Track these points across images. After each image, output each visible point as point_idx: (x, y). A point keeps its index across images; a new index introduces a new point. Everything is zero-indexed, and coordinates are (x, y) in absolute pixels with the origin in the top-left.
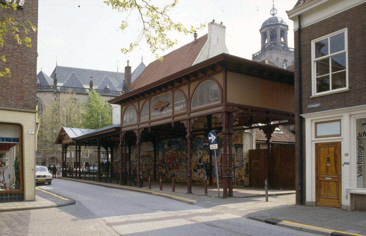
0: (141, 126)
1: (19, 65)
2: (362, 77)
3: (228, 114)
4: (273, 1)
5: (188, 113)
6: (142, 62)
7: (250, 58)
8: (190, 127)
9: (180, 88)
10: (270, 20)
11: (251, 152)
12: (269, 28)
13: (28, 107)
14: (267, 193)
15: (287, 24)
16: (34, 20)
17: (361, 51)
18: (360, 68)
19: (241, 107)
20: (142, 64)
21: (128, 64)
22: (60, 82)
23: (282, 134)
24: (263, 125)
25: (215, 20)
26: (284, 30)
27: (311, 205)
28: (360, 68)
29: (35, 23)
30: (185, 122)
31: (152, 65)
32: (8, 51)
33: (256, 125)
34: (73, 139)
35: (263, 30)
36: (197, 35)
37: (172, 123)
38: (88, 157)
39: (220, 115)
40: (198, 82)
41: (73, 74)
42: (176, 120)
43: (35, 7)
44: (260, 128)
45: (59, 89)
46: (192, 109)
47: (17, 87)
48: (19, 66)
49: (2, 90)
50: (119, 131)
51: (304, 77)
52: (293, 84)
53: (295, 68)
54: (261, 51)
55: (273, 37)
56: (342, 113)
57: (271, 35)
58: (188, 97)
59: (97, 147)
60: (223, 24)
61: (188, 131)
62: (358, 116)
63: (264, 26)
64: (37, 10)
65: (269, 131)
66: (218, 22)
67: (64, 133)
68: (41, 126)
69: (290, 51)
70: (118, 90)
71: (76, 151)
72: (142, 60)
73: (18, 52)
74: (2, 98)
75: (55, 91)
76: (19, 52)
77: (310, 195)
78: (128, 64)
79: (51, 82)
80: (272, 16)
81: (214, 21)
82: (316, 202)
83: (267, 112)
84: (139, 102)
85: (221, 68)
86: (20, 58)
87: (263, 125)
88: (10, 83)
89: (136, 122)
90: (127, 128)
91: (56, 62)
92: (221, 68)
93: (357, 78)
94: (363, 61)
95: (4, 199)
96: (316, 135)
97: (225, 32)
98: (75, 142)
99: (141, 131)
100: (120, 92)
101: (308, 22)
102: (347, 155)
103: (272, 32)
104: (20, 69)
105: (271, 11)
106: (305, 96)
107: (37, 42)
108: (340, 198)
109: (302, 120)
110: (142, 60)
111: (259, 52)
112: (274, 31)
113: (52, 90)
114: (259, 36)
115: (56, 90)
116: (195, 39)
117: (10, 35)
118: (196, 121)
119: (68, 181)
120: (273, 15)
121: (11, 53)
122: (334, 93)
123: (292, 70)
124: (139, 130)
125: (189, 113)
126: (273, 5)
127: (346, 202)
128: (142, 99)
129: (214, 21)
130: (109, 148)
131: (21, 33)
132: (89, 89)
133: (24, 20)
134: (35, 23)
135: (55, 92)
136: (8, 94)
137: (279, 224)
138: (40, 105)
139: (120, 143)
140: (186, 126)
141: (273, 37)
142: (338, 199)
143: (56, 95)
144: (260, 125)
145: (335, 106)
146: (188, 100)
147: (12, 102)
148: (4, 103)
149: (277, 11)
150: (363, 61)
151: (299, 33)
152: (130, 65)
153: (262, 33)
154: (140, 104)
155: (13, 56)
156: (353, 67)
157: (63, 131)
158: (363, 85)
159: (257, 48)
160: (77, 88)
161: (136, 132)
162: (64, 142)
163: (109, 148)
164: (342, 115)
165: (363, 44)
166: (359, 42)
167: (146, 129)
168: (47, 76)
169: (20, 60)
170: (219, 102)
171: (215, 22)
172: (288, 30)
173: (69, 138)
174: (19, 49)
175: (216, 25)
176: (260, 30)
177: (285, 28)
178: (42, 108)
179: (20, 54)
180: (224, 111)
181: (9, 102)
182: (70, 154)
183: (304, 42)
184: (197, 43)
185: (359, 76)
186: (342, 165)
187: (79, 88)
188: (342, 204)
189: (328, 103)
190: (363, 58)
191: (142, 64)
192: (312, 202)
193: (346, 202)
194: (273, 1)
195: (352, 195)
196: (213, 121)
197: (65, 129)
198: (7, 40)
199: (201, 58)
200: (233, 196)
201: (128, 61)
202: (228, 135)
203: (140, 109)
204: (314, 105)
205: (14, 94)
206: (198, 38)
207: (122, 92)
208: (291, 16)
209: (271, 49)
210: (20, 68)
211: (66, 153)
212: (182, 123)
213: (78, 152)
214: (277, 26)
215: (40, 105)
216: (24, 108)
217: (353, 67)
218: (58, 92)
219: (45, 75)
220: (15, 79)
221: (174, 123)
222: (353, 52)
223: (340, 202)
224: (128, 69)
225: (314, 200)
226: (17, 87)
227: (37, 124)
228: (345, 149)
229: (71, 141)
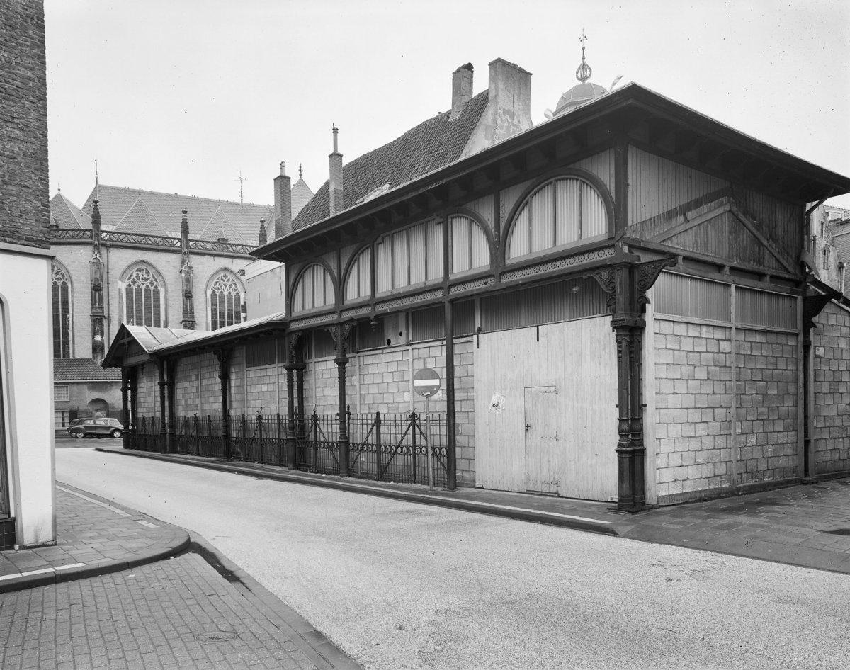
0: (347, 316)
4: (583, 49)
5: (446, 287)
6: (301, 179)
9: (577, 165)
14: (166, 383)
22: (108, 223)
40: (528, 183)
41: (140, 201)
42: (380, 311)
45: (106, 239)
50: (284, 330)
58: (342, 274)
67: (126, 340)
72: (301, 175)
75: (96, 242)
79: (86, 224)
80: (580, 83)
89: (333, 306)
91: (95, 175)
96: (66, 355)
105: (577, 72)
110: (301, 175)
113: (90, 240)
115: (98, 241)
120: (583, 79)
122: (558, 274)
126: (583, 59)
132: (179, 239)
135: (96, 245)
138: (59, 276)
143: (99, 252)
146: (338, 283)
149: (591, 70)
152: (287, 174)
154: (342, 264)
160: (151, 236)
162: (131, 361)
168: (75, 207)
173: (141, 350)
178: (64, 283)
187: (156, 237)
194: (583, 49)
199: (479, 144)
203: (503, 225)
213: (166, 387)
215: (59, 276)
218: (103, 245)
219: (72, 205)
229: (143, 358)
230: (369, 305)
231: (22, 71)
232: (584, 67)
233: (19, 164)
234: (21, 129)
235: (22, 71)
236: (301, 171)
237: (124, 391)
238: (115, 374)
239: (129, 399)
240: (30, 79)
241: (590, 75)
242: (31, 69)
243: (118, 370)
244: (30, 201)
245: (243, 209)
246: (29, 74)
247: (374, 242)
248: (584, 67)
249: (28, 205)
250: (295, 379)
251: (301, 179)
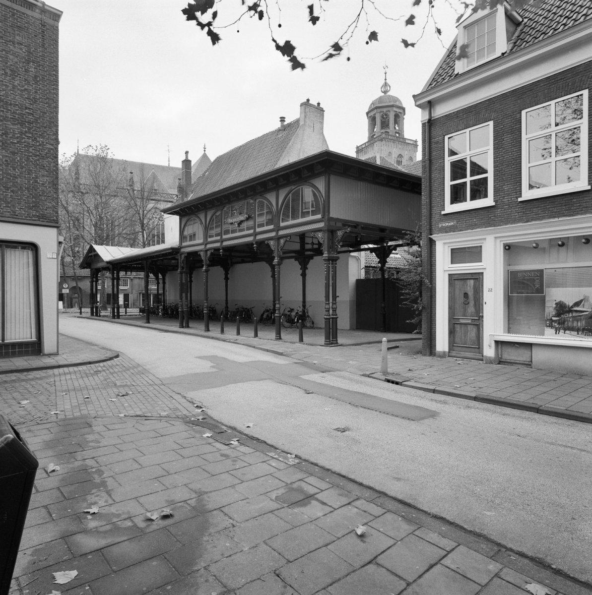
0: (209, 246)
1: (31, 156)
2: (512, 187)
3: (332, 232)
4: (386, 73)
6: (205, 153)
7: (351, 153)
8: (278, 249)
9: (310, 181)
10: (380, 99)
11: (359, 282)
12: (379, 110)
13: (45, 219)
15: (404, 106)
16: (52, 91)
17: (510, 153)
18: (509, 176)
19: (346, 223)
20: (205, 156)
21: (187, 156)
23: (399, 258)
24: (376, 246)
25: (310, 99)
26: (400, 114)
27: (443, 355)
28: (509, 176)
29: (55, 96)
30: (272, 243)
31: (219, 159)
32: (13, 135)
33: (366, 246)
34: (108, 263)
35: (372, 114)
36: (285, 119)
37: (254, 243)
38: (128, 287)
39: (320, 235)
43: (54, 70)
44: (372, 250)
46: (282, 224)
47: (28, 189)
48: (31, 158)
49: (4, 193)
51: (435, 185)
52: (420, 194)
53: (424, 172)
54: (367, 142)
55: (385, 124)
56: (487, 234)
57: (381, 120)
59: (143, 274)
60: (321, 106)
61: (275, 254)
62: (506, 239)
63: (373, 107)
64: (57, 76)
65: (383, 254)
66: (313, 102)
67: (93, 254)
68: (66, 249)
69: (407, 143)
70: (171, 193)
71: (113, 279)
72: (205, 151)
73: (29, 138)
74: (4, 205)
76: (30, 137)
77: (442, 343)
78: (187, 156)
80: (383, 94)
81: (308, 100)
82: (449, 352)
83: (382, 229)
84: (206, 212)
85: (323, 170)
86: (31, 147)
87: (376, 246)
88: (17, 182)
90: (187, 248)
92: (323, 170)
93: (506, 189)
94: (513, 167)
95: (16, 353)
97: (323, 115)
98: (111, 266)
99: (209, 253)
100: (174, 195)
101: (441, 111)
102: (490, 290)
103: (382, 117)
104: (32, 163)
105: (381, 88)
106: (435, 210)
107: (58, 123)
108: (481, 347)
109: (432, 243)
110: (205, 151)
111: (365, 143)
112: (386, 115)
114: (365, 122)
116: (282, 126)
117: (15, 111)
118: (286, 241)
119: (96, 321)
120: (385, 92)
121: (17, 138)
123: (418, 172)
124: (206, 251)
125: (278, 231)
126: (386, 80)
127: (489, 351)
128: (210, 208)
129: (308, 100)
130: (160, 275)
131: (32, 109)
133: (37, 90)
134: (55, 96)
136: (15, 198)
137: (403, 384)
139: (179, 268)
140: (273, 248)
141: (385, 124)
142: (479, 348)
144: (371, 246)
145: (476, 225)
147: (21, 211)
148: (9, 212)
149: (390, 87)
150: (513, 167)
151: (430, 126)
152: (189, 158)
153: (370, 117)
155: (22, 142)
156: (500, 174)
157: (92, 249)
158: (513, 199)
159: (363, 137)
161: (202, 254)
163: (160, 275)
164: (484, 237)
165: (513, 144)
166: (508, 140)
167: (217, 250)
169: (33, 149)
170: (319, 216)
171: (310, 102)
172: (404, 114)
173: (102, 260)
174: (30, 133)
175: (311, 105)
176: (367, 114)
177: (401, 111)
179: (33, 140)
180: (326, 229)
181: (17, 211)
182: (106, 284)
183: (435, 139)
184: (284, 130)
185: (508, 186)
186: (484, 303)
188: (484, 355)
189: (467, 221)
190: (513, 162)
191: (205, 156)
192: (444, 352)
193: (489, 351)
194: (386, 73)
195: (497, 342)
196: (308, 240)
197: (96, 247)
198: (11, 118)
200: (337, 343)
201: (187, 153)
202: (331, 262)
204: (447, 224)
205: (24, 200)
206: (285, 123)
207: (177, 196)
208: (418, 103)
209: (382, 140)
210: (32, 161)
211: (97, 281)
212: (268, 244)
213: (115, 281)
214: (389, 109)
216: (40, 221)
217: (500, 174)
220: (25, 177)
221: (256, 243)
222: (500, 154)
223: (481, 352)
224: (187, 163)
225: (447, 350)
226: (28, 189)
227: (60, 243)
228: (488, 283)
230: (203, 244)
231: (49, 146)
232: (386, 84)
233: (46, 187)
234: (47, 171)
235: (49, 146)
236: (205, 148)
237: (92, 282)
238: (87, 272)
239: (331, 288)
240: (52, 149)
241: (389, 90)
242: (52, 145)
243: (88, 270)
244: (50, 202)
245: (168, 169)
246: (52, 147)
247: (222, 210)
248: (386, 84)
249: (50, 205)
250: (115, 283)
251: (205, 153)
